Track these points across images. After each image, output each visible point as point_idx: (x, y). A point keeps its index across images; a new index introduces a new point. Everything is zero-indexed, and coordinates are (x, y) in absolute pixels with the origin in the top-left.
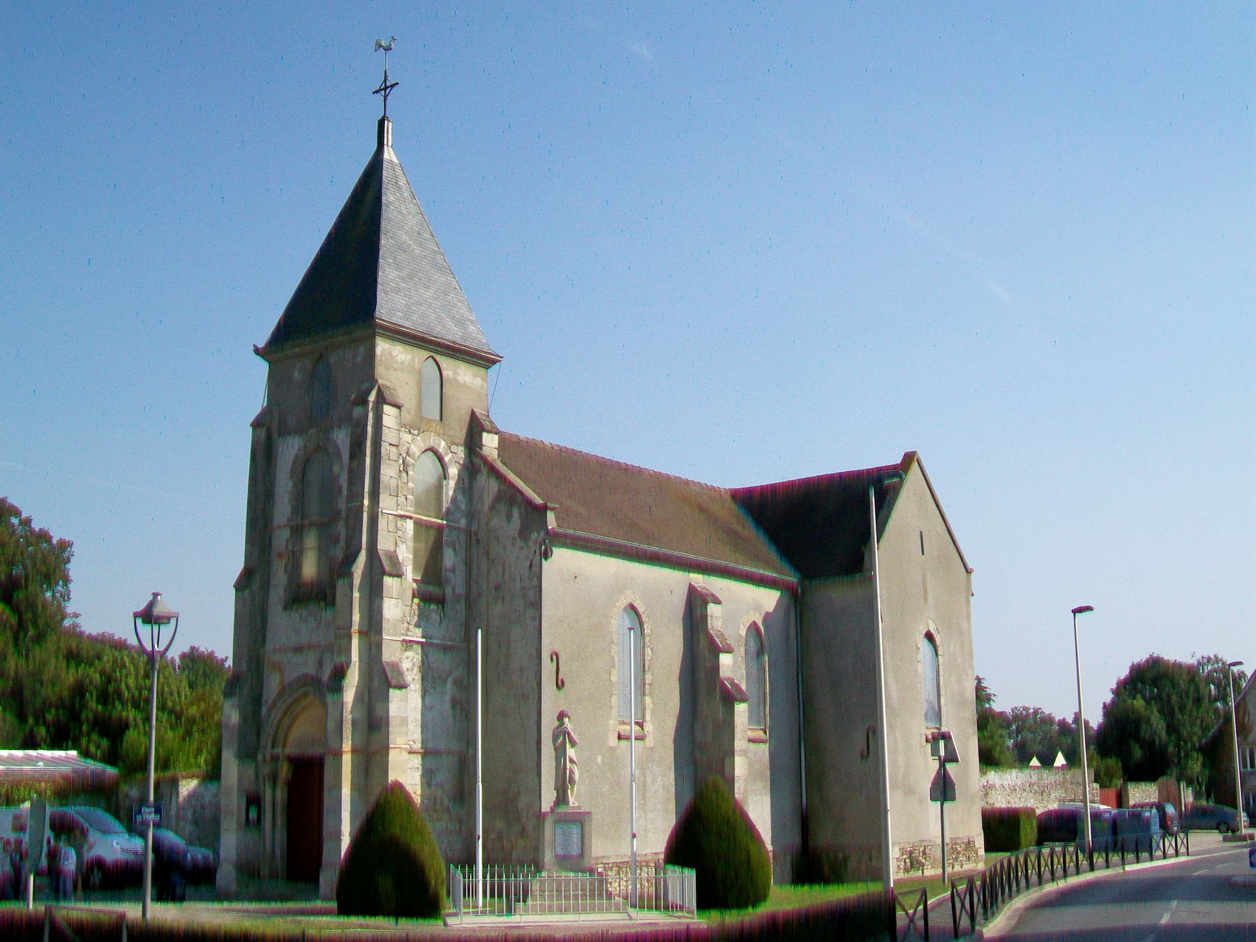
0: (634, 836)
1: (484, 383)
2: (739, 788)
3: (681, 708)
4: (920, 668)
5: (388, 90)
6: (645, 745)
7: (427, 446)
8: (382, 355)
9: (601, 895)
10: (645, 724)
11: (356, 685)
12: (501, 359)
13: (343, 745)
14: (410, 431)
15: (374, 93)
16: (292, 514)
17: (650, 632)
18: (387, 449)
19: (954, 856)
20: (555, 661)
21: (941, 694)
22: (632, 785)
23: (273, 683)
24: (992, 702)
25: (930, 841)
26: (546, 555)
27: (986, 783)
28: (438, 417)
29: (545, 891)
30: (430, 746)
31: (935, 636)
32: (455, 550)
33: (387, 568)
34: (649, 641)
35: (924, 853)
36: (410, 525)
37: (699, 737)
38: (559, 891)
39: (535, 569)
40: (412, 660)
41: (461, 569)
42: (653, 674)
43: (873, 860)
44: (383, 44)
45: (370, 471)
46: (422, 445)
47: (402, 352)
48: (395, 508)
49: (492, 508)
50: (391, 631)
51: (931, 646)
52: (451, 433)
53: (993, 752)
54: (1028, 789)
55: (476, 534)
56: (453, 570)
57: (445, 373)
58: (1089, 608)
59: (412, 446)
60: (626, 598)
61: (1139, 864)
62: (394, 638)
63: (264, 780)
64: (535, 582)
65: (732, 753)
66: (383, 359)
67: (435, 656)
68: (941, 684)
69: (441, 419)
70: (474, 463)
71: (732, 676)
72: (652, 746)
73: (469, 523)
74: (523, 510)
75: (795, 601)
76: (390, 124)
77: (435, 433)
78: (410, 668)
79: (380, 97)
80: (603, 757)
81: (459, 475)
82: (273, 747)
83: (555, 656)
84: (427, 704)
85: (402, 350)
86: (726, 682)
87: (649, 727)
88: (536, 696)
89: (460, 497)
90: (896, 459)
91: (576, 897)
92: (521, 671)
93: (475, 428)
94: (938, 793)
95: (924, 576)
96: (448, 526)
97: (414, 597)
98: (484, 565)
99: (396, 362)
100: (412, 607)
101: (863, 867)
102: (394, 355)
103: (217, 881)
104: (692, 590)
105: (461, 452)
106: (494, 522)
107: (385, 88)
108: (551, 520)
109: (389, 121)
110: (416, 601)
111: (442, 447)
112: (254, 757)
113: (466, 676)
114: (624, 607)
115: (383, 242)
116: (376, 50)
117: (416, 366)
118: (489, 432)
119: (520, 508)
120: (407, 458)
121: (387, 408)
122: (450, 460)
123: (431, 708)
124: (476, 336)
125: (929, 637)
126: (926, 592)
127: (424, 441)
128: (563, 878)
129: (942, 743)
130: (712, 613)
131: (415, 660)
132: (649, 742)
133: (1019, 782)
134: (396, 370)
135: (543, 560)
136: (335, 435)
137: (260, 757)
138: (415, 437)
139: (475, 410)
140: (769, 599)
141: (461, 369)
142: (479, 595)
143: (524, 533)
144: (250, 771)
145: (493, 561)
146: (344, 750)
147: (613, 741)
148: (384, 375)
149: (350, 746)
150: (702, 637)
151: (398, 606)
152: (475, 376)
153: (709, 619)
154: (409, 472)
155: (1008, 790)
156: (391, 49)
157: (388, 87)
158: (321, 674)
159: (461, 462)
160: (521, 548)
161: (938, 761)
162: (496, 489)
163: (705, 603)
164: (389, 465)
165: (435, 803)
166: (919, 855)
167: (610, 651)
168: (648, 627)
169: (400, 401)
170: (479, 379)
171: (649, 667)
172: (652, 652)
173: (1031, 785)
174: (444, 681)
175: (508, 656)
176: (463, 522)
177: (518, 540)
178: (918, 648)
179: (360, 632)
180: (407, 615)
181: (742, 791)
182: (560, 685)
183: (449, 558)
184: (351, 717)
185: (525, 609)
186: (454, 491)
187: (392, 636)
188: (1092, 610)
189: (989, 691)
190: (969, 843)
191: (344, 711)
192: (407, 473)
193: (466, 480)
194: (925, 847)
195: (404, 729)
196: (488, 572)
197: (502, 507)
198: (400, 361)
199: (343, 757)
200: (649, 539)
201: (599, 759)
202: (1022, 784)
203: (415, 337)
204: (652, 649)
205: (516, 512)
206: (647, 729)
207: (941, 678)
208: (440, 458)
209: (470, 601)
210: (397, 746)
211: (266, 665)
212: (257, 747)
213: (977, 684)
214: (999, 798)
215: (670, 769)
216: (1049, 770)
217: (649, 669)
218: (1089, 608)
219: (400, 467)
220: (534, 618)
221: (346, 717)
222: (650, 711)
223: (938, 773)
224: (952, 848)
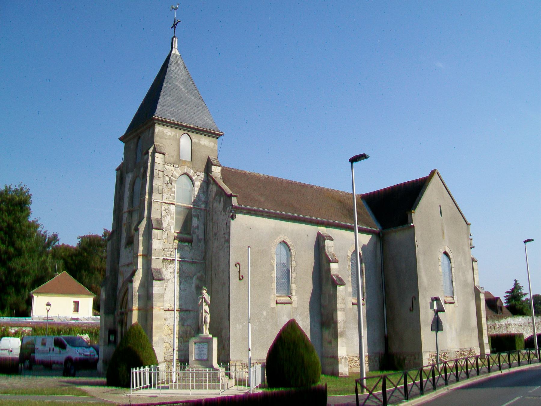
0: (249, 350)
1: (215, 145)
2: (340, 327)
3: (313, 289)
4: (440, 269)
6: (292, 306)
7: (183, 172)
8: (158, 133)
9: (214, 380)
10: (292, 297)
11: (140, 279)
12: (223, 134)
13: (133, 307)
14: (173, 166)
15: (171, 28)
17: (295, 254)
18: (157, 173)
21: (453, 281)
22: (249, 325)
24: (522, 290)
25: (448, 350)
26: (233, 218)
27: (506, 323)
28: (190, 161)
29: (198, 378)
30: (184, 307)
31: (449, 254)
32: (198, 219)
33: (154, 226)
34: (294, 258)
35: (444, 356)
37: (323, 302)
38: (193, 377)
39: (228, 224)
41: (202, 227)
42: (296, 273)
43: (416, 359)
44: (174, 7)
45: (149, 183)
46: (180, 172)
47: (170, 131)
48: (161, 199)
49: (214, 199)
50: (157, 255)
51: (448, 258)
52: (196, 167)
53: (523, 310)
54: (527, 325)
55: (209, 211)
56: (197, 227)
57: (193, 140)
58: (531, 240)
59: (175, 172)
60: (280, 238)
61: (521, 367)
62: (158, 258)
64: (228, 230)
65: (336, 309)
66: (159, 134)
67: (186, 266)
68: (453, 276)
69: (191, 161)
70: (209, 180)
71: (338, 274)
73: (206, 207)
74: (224, 198)
75: (380, 238)
76: (176, 40)
77: (188, 166)
78: (172, 272)
79: (173, 29)
80: (267, 312)
81: (201, 185)
82: (121, 309)
83: (238, 264)
84: (182, 288)
85: (169, 130)
86: (333, 276)
87: (294, 298)
88: (228, 283)
89: (201, 195)
90: (427, 174)
91: (201, 380)
92: (223, 272)
93: (209, 164)
94: (434, 328)
95: (442, 226)
96: (193, 208)
97: (174, 239)
99: (166, 135)
100: (173, 244)
101: (412, 362)
103: (98, 368)
104: (319, 234)
105: (202, 175)
106: (215, 204)
108: (235, 202)
109: (175, 38)
110: (176, 241)
111: (191, 172)
112: (113, 313)
113: (204, 276)
115: (165, 85)
116: (171, 10)
117: (177, 137)
118: (215, 165)
120: (172, 177)
121: (157, 155)
122: (196, 179)
123: (184, 290)
124: (211, 126)
125: (446, 254)
126: (443, 233)
127: (181, 170)
129: (435, 303)
130: (328, 245)
132: (294, 305)
133: (523, 322)
134: (166, 139)
135: (231, 220)
137: (116, 313)
138: (176, 168)
139: (210, 156)
140: (365, 239)
141: (203, 139)
143: (224, 209)
144: (111, 319)
145: (214, 222)
146: (133, 309)
147: (273, 305)
148: (158, 141)
149: (137, 308)
150: (323, 255)
151: (161, 243)
152: (210, 142)
153: (326, 247)
154: (173, 184)
155: (518, 325)
156: (177, 9)
158: (161, 277)
159: (202, 179)
161: (434, 311)
162: (216, 189)
163: (325, 240)
164: (158, 180)
165: (186, 333)
166: (441, 357)
167: (271, 263)
168: (293, 252)
169: (164, 152)
170: (213, 143)
171: (294, 270)
172: (296, 263)
173: (529, 323)
174: (192, 278)
175: (219, 265)
176: (203, 206)
178: (439, 260)
179: (143, 255)
180: (171, 248)
181: (342, 328)
182: (241, 278)
183: (195, 222)
184: (137, 294)
185: (224, 243)
186: (198, 192)
187: (157, 257)
188: (533, 241)
189: (520, 285)
190: (471, 350)
191: (134, 291)
192: (172, 184)
193: (205, 187)
194: (445, 353)
195: (162, 299)
196: (212, 228)
197: (217, 197)
198: (168, 135)
199: (133, 312)
200: (295, 210)
201: (265, 313)
202: (525, 323)
203: (176, 124)
205: (222, 199)
206: (293, 299)
207: (453, 274)
208: (191, 178)
209: (206, 241)
210: (158, 307)
212: (115, 309)
213: (515, 282)
214: (514, 329)
215: (307, 318)
216: (538, 317)
217: (294, 271)
218: (531, 240)
219: (168, 181)
220: (227, 247)
221: (135, 294)
222: (295, 291)
223: (434, 318)
224: (461, 353)
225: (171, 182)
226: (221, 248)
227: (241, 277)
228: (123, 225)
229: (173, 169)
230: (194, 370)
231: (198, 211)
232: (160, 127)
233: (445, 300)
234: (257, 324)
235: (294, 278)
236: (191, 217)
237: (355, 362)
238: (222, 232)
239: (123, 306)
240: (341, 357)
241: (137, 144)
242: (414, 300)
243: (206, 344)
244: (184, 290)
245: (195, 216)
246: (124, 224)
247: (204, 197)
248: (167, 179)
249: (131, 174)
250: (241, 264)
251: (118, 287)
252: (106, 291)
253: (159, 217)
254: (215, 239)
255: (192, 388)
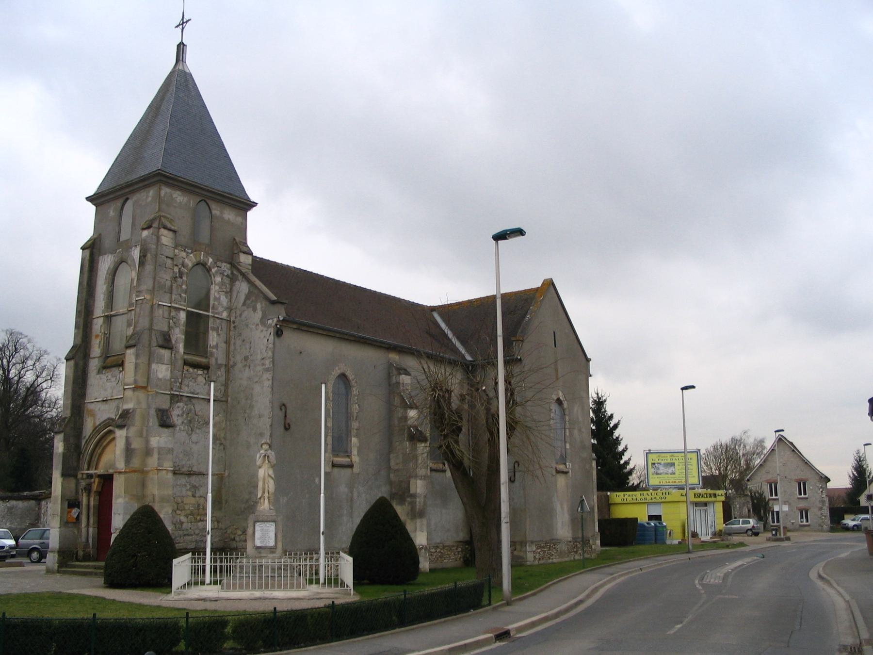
5: (184, 25)
16: (105, 308)
17: (358, 393)
18: (164, 261)
19: (575, 550)
20: (284, 410)
23: (89, 426)
25: (558, 540)
34: (357, 399)
36: (183, 316)
40: (182, 409)
42: (359, 422)
47: (180, 196)
49: (244, 304)
56: (216, 347)
59: (186, 260)
63: (82, 491)
66: (166, 199)
72: (357, 472)
73: (229, 315)
79: (179, 29)
98: (239, 342)
102: (174, 197)
107: (183, 23)
114: (338, 375)
119: (261, 304)
122: (216, 272)
125: (559, 402)
127: (195, 256)
128: (270, 563)
131: (184, 409)
132: (356, 469)
134: (175, 207)
136: (133, 252)
142: (235, 364)
157: (184, 23)
160: (262, 331)
171: (357, 417)
172: (359, 407)
177: (260, 326)
187: (163, 390)
198: (179, 201)
204: (359, 405)
205: (259, 306)
209: (228, 368)
210: (164, 468)
211: (85, 412)
212: (78, 468)
219: (176, 274)
225: (181, 275)
226: (256, 379)
227: (287, 426)
228: (93, 338)
229: (184, 254)
230: (256, 563)
231: (218, 321)
232: (167, 189)
233: (556, 468)
234: (307, 496)
235: (356, 429)
236: (208, 331)
237: (432, 555)
238: (259, 357)
239: (91, 465)
240: (420, 547)
241: (122, 209)
242: (516, 466)
243: (272, 523)
244: (196, 443)
245: (213, 329)
246: (97, 336)
247: (227, 301)
248: (176, 270)
249: (110, 257)
250: (288, 405)
251: (84, 435)
252: (65, 440)
253: (166, 329)
254: (245, 366)
255: (265, 588)
